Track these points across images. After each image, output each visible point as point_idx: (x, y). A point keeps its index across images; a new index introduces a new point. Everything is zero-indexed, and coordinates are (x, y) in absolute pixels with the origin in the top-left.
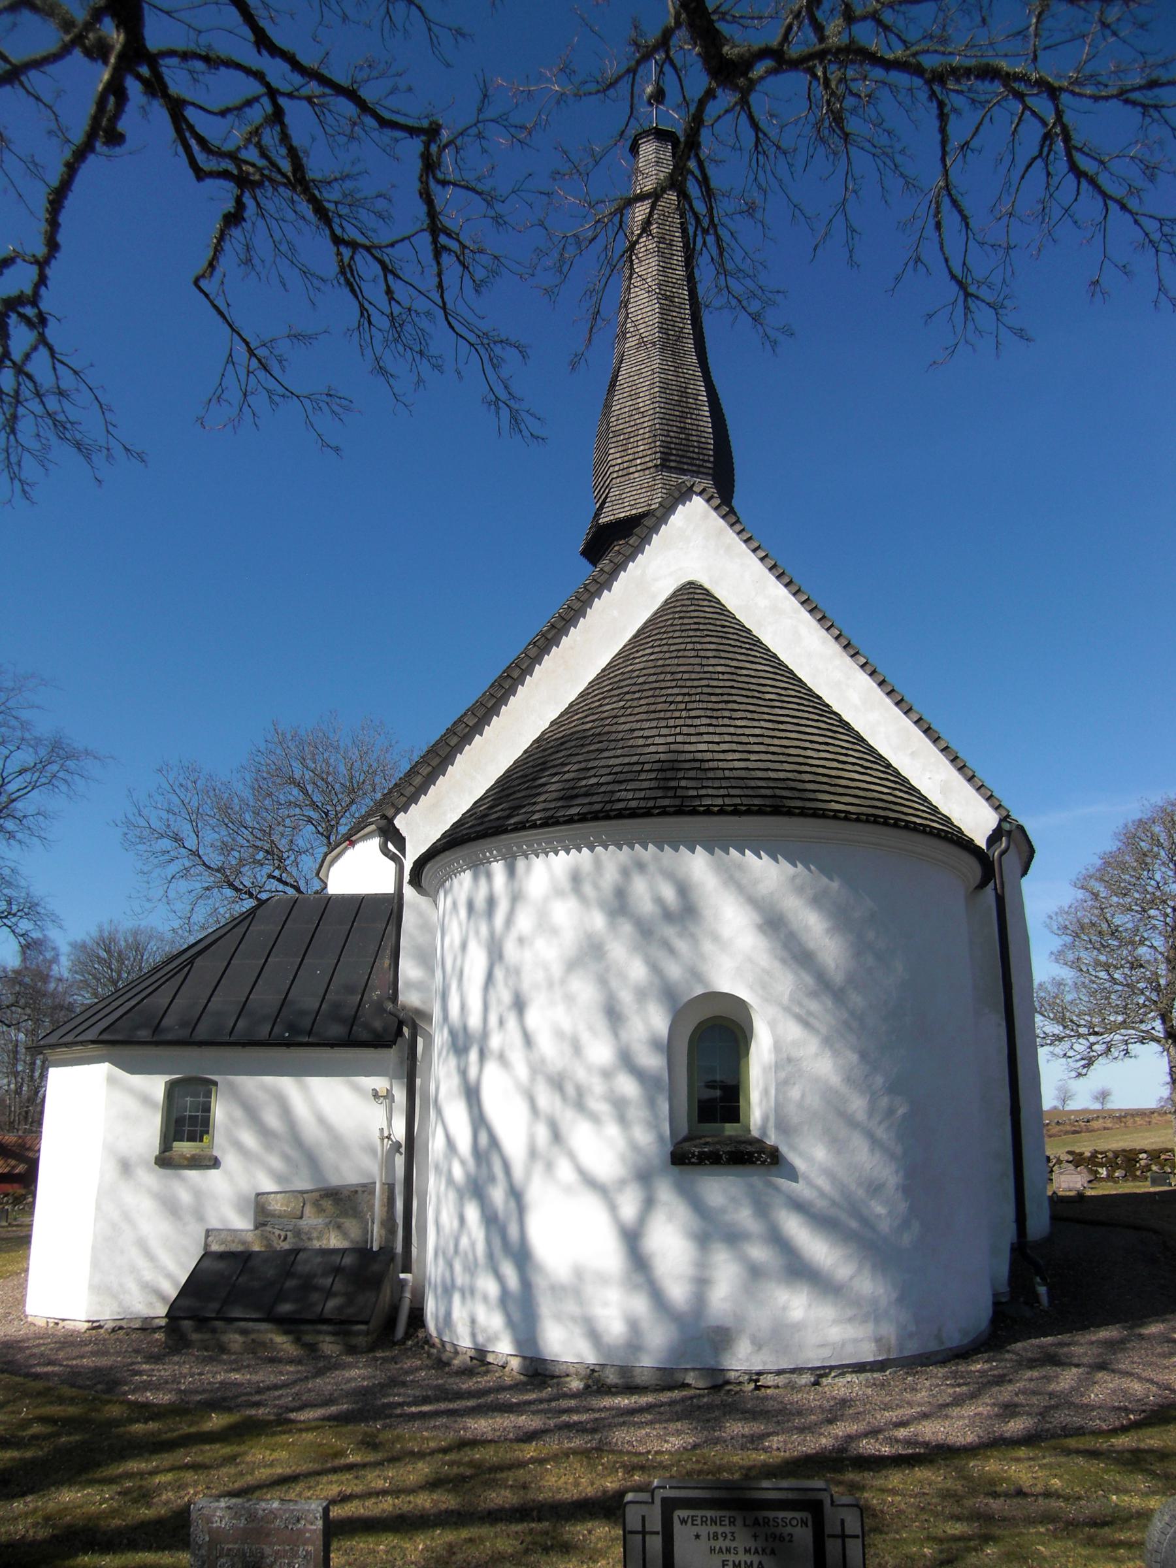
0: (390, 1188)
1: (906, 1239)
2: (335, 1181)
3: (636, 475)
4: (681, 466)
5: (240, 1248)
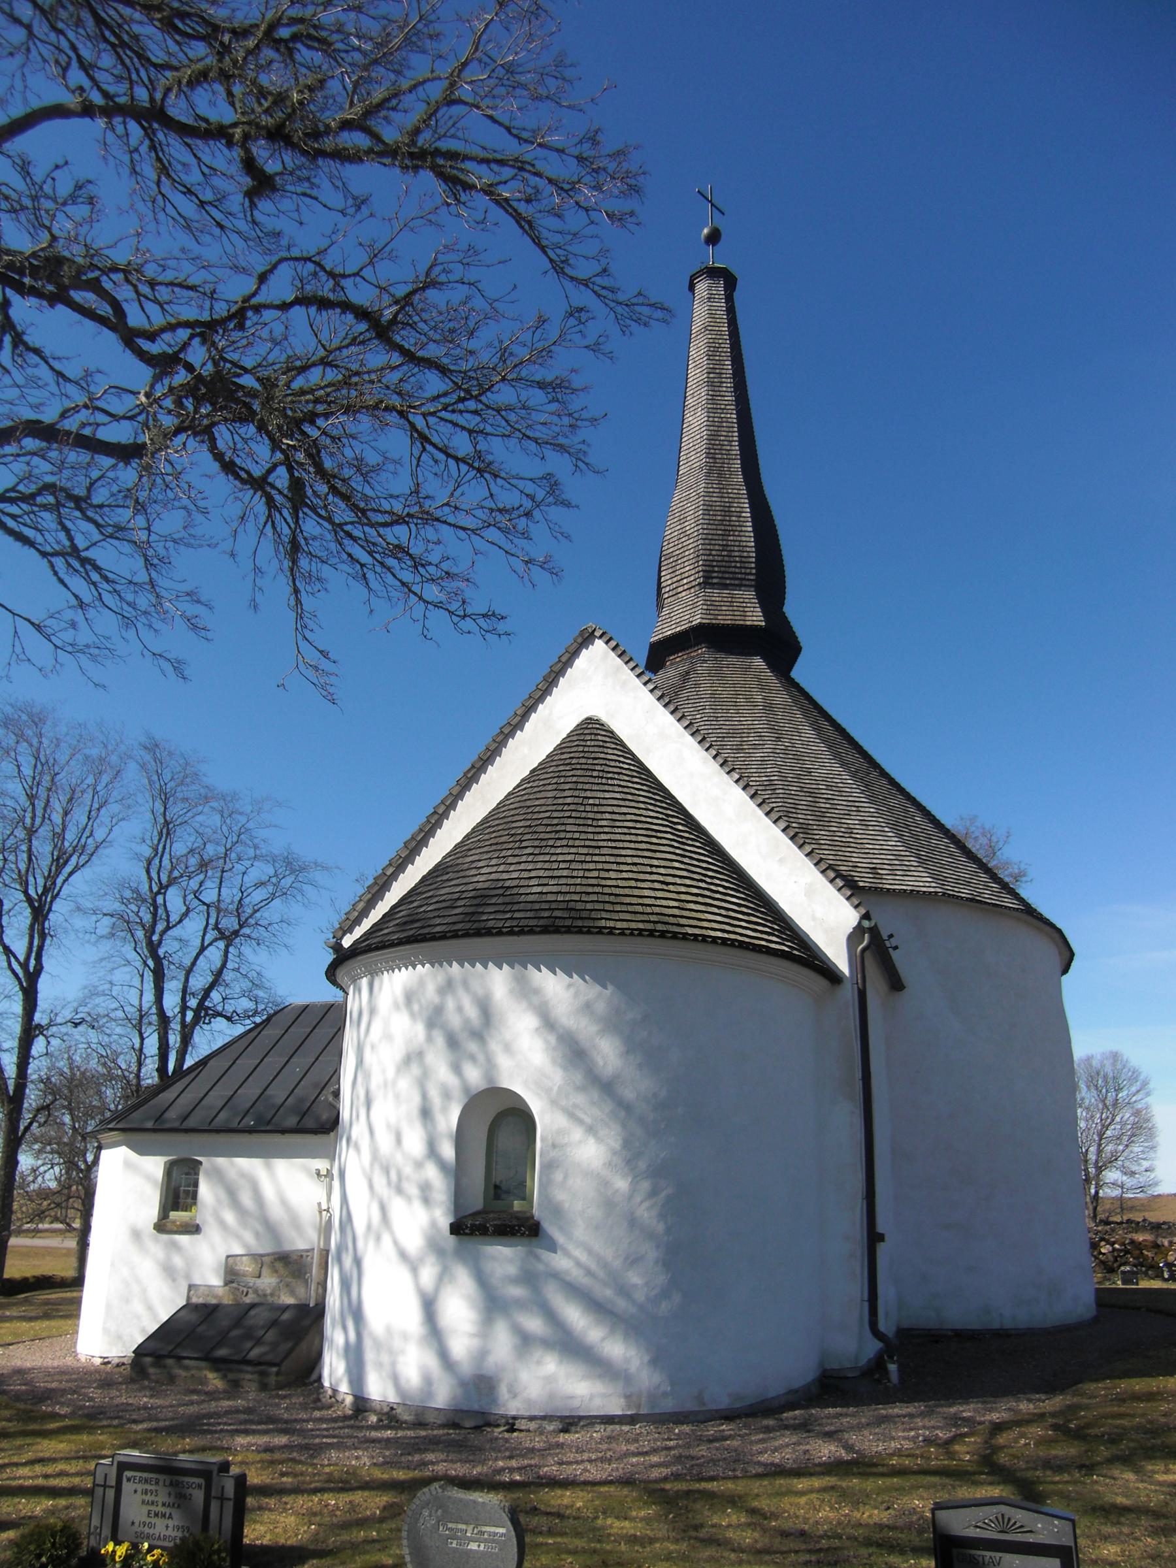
1: (664, 1307)
2: (288, 1247)
3: (684, 594)
4: (724, 581)
5: (214, 1301)
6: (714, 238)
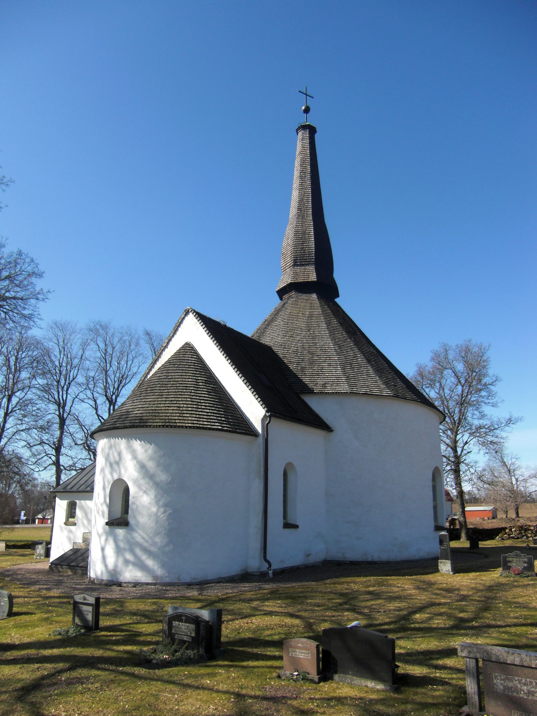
1: (167, 549)
6: (307, 110)
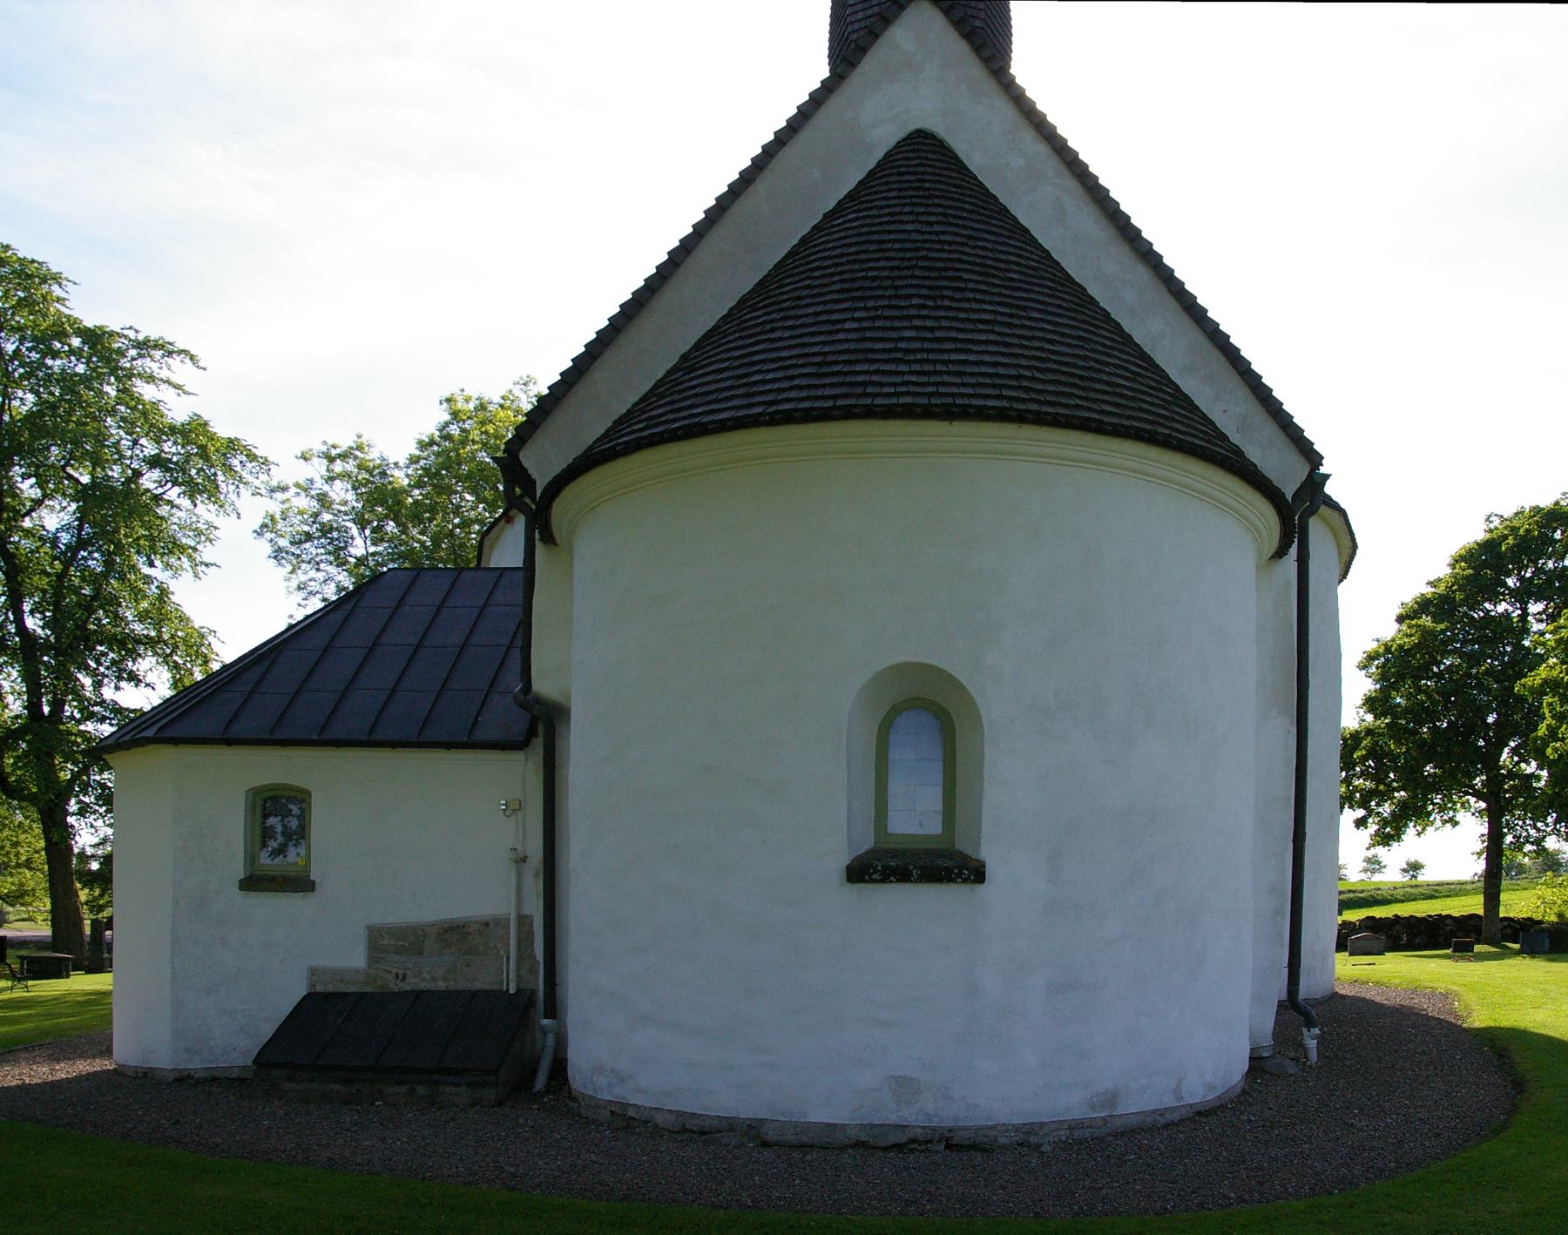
0: (524, 921)
